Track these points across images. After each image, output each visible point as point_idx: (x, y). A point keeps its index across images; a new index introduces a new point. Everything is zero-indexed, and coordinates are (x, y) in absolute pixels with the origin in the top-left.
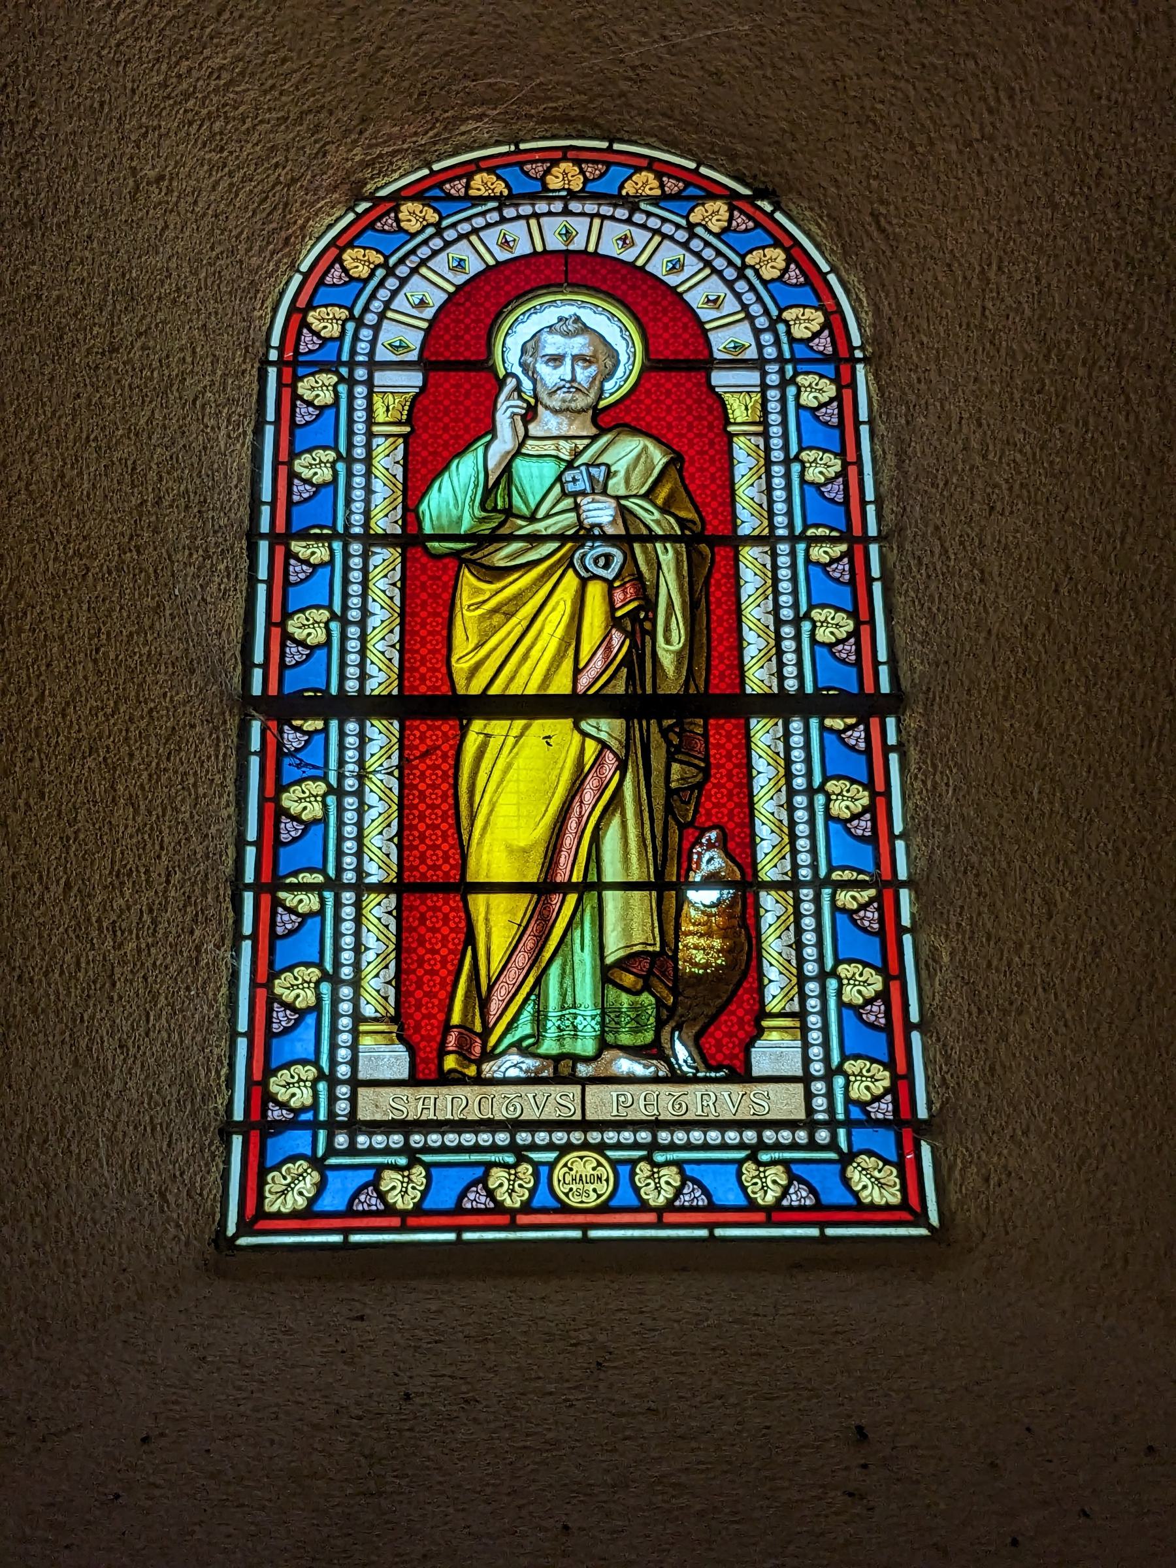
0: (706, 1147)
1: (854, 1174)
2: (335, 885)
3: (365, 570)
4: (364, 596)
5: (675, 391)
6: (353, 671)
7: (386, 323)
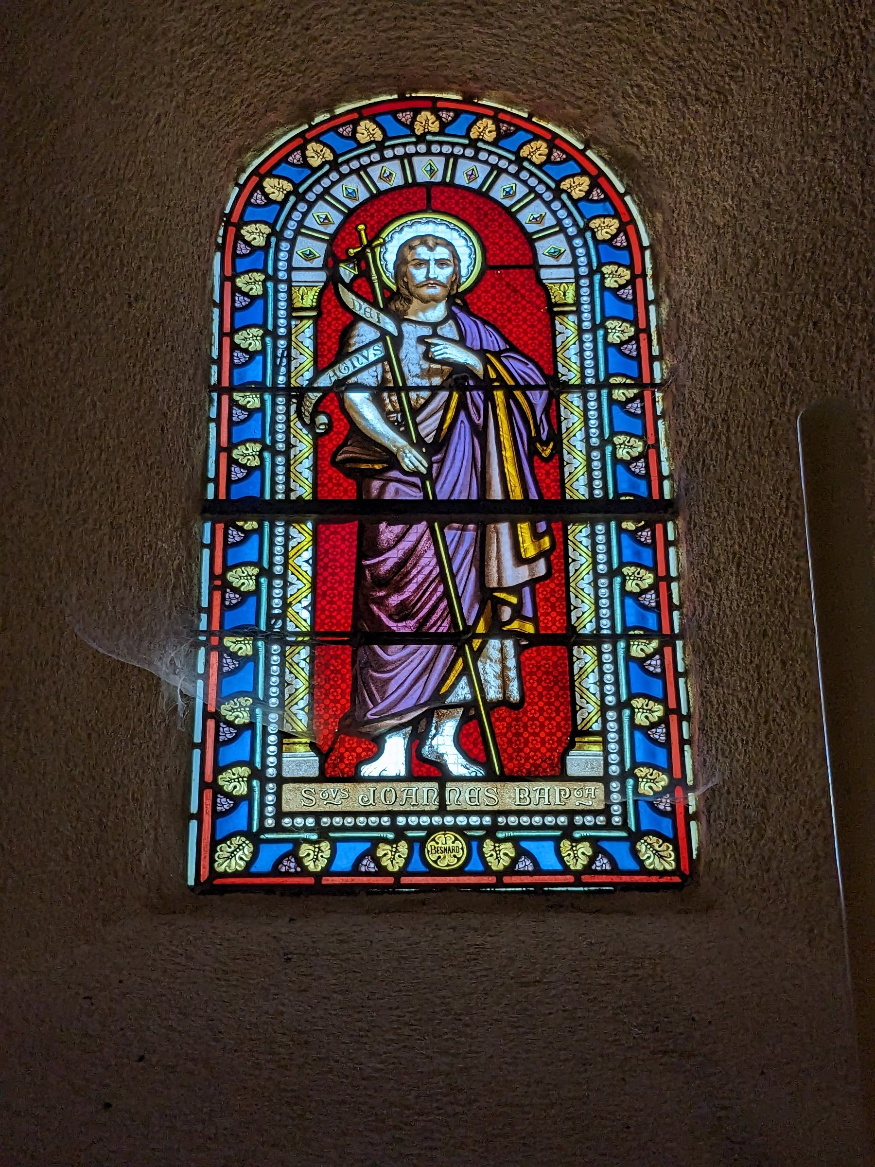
0: (531, 827)
1: (641, 847)
2: (269, 637)
3: (598, 618)
4: (597, 598)
5: (507, 293)
6: (601, 538)
7: (300, 238)
